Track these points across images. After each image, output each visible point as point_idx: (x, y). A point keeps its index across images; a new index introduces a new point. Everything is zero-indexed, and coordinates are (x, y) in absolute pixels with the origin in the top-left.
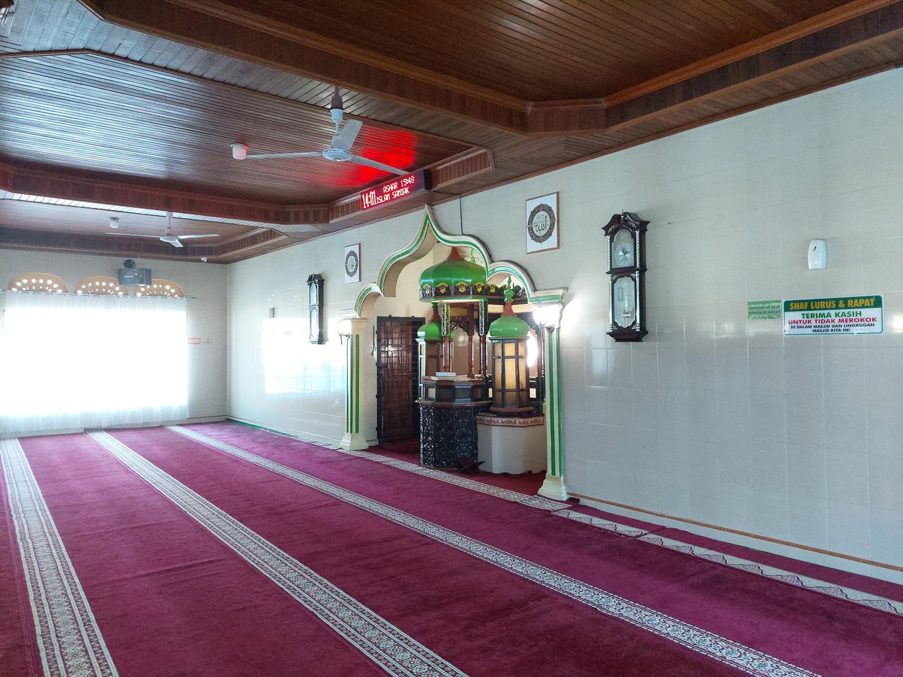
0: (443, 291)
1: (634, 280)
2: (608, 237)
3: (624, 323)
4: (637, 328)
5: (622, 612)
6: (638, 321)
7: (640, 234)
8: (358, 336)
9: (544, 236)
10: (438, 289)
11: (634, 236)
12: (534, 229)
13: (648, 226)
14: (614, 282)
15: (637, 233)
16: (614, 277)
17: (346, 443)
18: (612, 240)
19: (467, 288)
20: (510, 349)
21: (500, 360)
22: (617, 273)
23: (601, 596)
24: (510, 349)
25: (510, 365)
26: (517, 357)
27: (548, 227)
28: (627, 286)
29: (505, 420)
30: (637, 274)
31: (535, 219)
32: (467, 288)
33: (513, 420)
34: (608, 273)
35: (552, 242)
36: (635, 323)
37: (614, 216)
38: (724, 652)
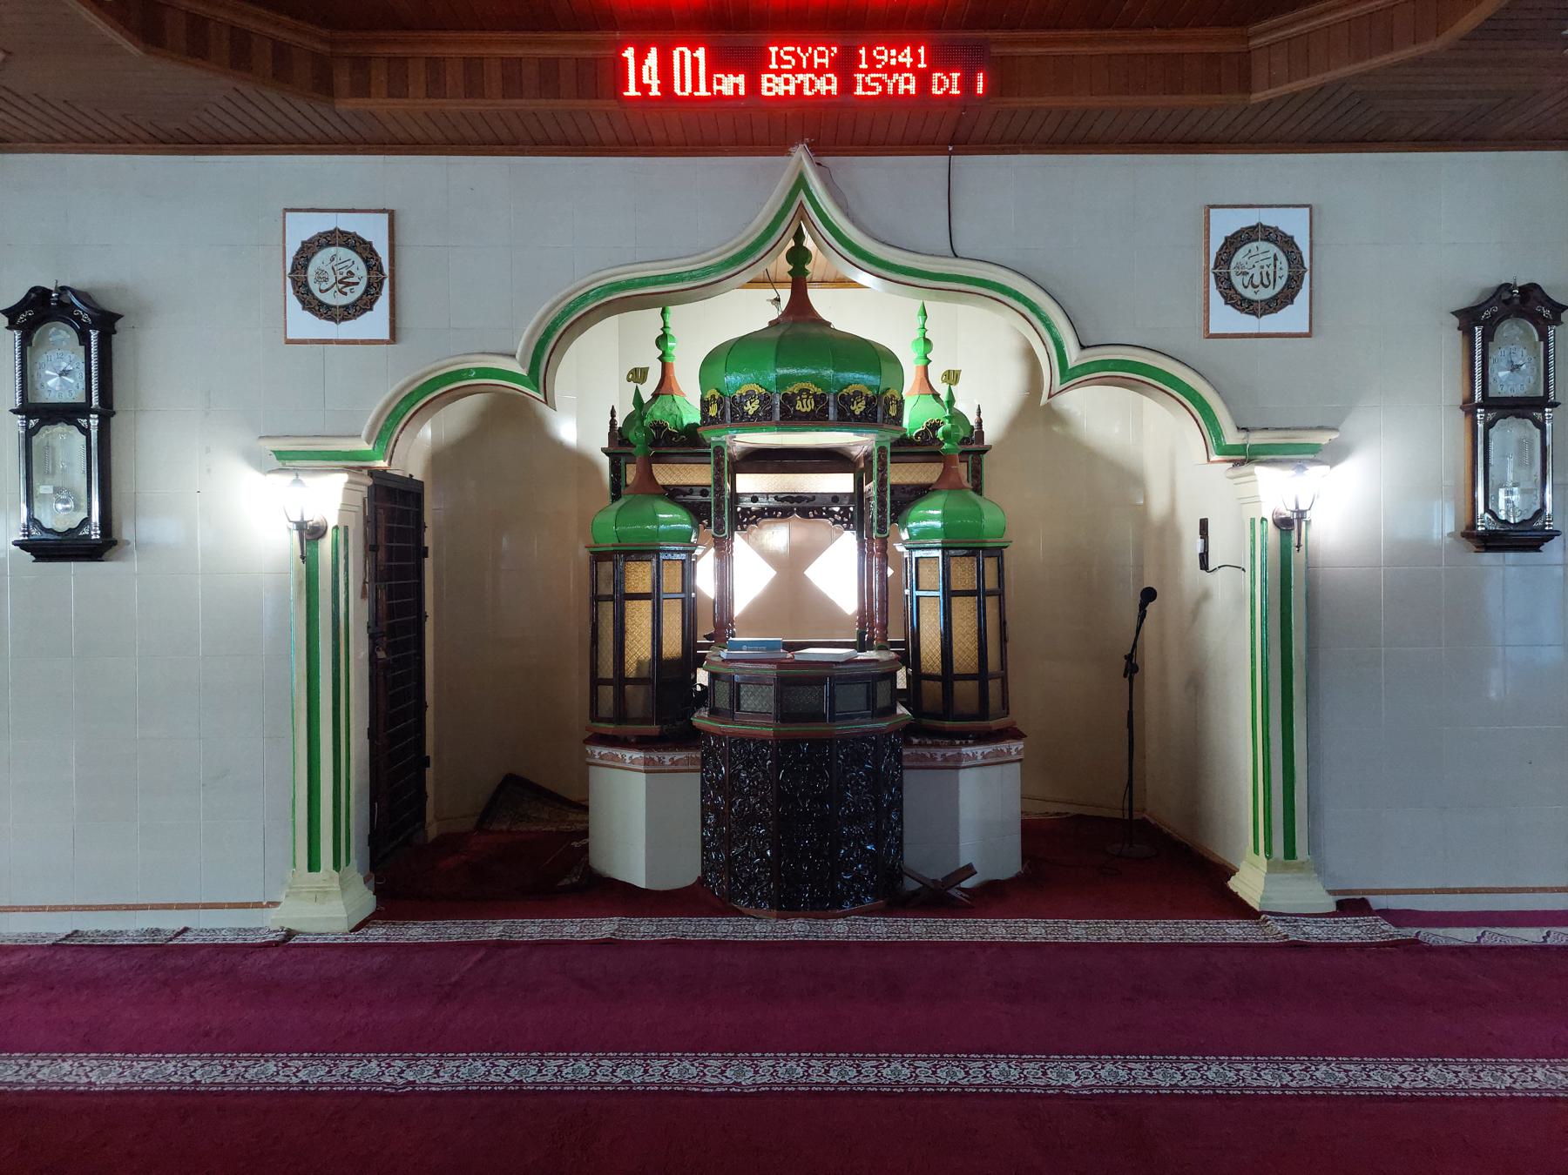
0: (751, 408)
1: (86, 431)
2: (17, 334)
3: (58, 517)
4: (96, 535)
5: (197, 1076)
6: (95, 518)
7: (100, 337)
8: (346, 528)
9: (1268, 302)
10: (788, 399)
11: (84, 339)
12: (1237, 281)
13: (119, 324)
14: (30, 434)
15: (94, 335)
16: (32, 423)
17: (324, 905)
18: (26, 341)
19: (820, 399)
20: (639, 577)
21: (646, 606)
22: (39, 414)
23: (34, 1065)
24: (639, 577)
25: (639, 617)
26: (655, 597)
27: (1281, 283)
28: (68, 447)
29: (987, 749)
30: (94, 421)
31: (1240, 257)
32: (820, 399)
33: (1003, 746)
34: (15, 412)
35: (1293, 317)
36: (86, 522)
37: (34, 290)
38: (513, 1073)
